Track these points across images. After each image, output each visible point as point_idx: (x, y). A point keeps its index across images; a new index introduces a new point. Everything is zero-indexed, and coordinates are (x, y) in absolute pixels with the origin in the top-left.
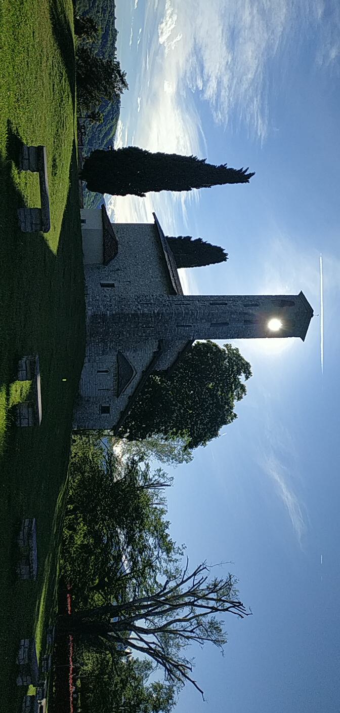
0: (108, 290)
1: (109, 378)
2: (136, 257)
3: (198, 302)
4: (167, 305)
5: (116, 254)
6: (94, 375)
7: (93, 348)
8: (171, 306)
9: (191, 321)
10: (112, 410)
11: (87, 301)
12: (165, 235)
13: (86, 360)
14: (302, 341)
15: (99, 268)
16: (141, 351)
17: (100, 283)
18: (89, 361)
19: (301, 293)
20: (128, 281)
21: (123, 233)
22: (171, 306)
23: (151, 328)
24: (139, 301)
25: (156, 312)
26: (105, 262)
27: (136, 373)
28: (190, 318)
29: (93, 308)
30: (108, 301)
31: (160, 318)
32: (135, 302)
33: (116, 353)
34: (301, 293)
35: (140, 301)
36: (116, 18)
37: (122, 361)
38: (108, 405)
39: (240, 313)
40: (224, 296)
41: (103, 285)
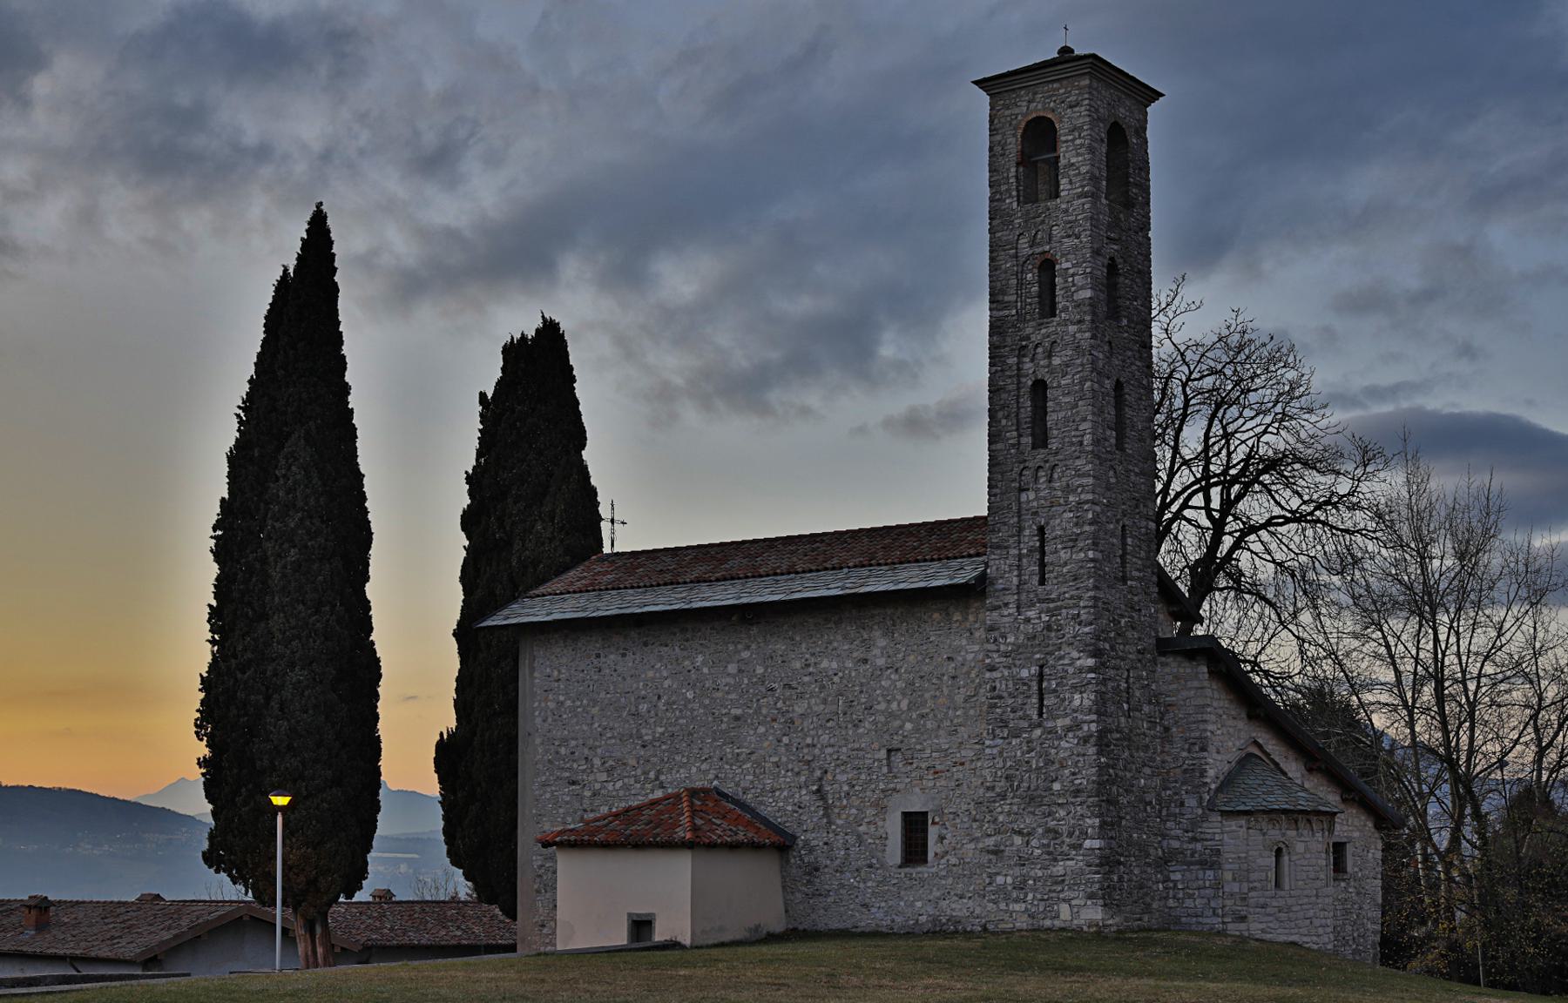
0: (942, 838)
1: (1300, 847)
2: (737, 718)
4: (1052, 613)
6: (1290, 901)
7: (1189, 903)
18: (1243, 919)
23: (1131, 680)
25: (1090, 662)
26: (782, 845)
27: (1256, 743)
34: (981, 83)
36: (1066, 50)
39: (1094, 337)
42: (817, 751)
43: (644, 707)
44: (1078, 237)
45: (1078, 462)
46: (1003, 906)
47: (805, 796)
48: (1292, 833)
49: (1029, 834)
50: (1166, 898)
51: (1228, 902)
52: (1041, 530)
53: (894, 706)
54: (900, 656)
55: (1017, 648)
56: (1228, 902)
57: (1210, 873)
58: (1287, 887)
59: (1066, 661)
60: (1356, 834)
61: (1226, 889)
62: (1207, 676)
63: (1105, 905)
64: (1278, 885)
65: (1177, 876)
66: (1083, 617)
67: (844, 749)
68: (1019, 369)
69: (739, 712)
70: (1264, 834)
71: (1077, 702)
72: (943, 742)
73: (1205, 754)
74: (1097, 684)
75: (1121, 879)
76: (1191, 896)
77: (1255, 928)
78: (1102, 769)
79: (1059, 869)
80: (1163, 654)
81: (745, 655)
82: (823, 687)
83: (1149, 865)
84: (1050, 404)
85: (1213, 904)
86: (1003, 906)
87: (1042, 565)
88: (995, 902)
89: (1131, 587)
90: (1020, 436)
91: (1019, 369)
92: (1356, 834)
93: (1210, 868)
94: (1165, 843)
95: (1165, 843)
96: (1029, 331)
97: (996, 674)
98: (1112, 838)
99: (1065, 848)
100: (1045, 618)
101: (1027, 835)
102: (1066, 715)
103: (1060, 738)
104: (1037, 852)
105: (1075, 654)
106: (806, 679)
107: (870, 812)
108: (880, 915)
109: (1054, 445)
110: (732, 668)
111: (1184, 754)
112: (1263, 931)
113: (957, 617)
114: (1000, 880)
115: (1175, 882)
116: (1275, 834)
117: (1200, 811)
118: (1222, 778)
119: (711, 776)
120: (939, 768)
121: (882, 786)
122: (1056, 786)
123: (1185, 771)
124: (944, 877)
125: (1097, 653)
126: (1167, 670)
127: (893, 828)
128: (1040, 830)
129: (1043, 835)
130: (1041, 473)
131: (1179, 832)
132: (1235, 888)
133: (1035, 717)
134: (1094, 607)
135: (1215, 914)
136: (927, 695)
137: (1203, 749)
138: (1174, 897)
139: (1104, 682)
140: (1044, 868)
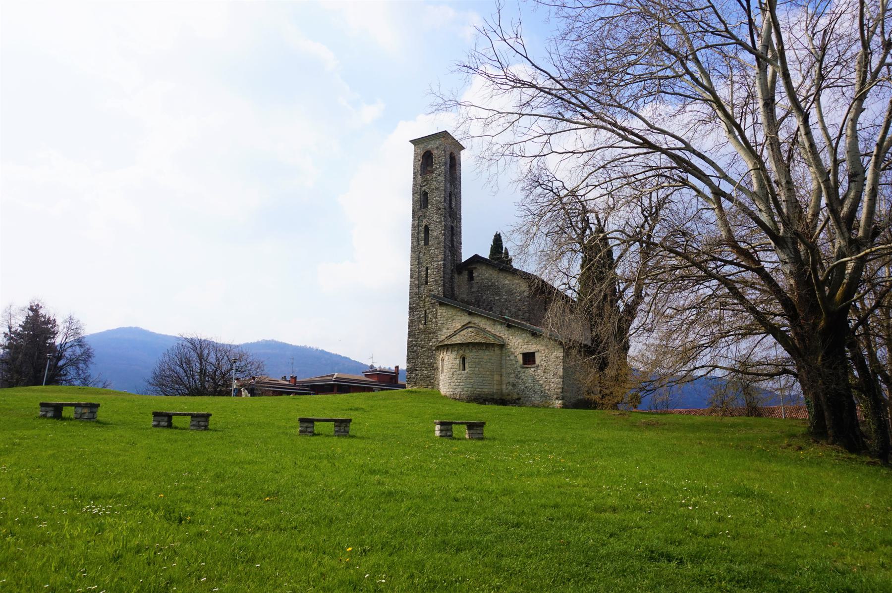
19: (414, 142)
34: (414, 142)
38: (521, 356)
75: (417, 375)
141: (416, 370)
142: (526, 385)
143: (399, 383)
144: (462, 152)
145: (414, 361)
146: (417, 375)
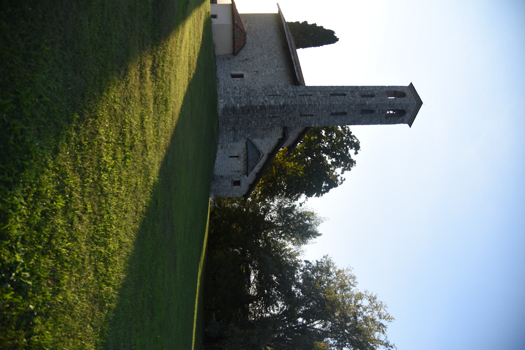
0: (238, 81)
1: (239, 162)
2: (262, 46)
3: (319, 93)
4: (292, 97)
5: (245, 44)
8: (295, 97)
9: (313, 111)
10: (243, 183)
11: (219, 93)
12: (286, 21)
13: (219, 146)
14: (409, 127)
15: (229, 59)
16: (268, 138)
17: (231, 74)
18: (222, 148)
19: (411, 84)
20: (255, 71)
21: (251, 23)
22: (295, 97)
23: (277, 118)
24: (266, 92)
25: (282, 104)
26: (235, 53)
27: (263, 155)
28: (312, 109)
29: (224, 101)
30: (238, 93)
31: (285, 109)
32: (262, 93)
33: (245, 141)
34: (411, 84)
35: (267, 92)
37: (250, 146)
38: (239, 180)
39: (358, 104)
40: (343, 87)
41: (234, 76)
42: (256, 59)
43: (263, 32)
44: (380, 101)
45: (328, 101)
46: (223, 90)
47: (245, 57)
48: (242, 160)
49: (240, 94)
50: (226, 131)
51: (225, 145)
52: (312, 95)
53: (267, 72)
54: (279, 72)
55: (284, 91)
56: (225, 145)
57: (232, 140)
58: (230, 159)
59: (281, 100)
60: (242, 189)
61: (229, 144)
62: (279, 138)
63: (224, 109)
64: (231, 157)
65: (231, 133)
66: (292, 103)
67: (257, 64)
68: (348, 91)
69: (263, 46)
70: (242, 153)
71: (272, 102)
72: (260, 80)
73: (260, 138)
74: (276, 106)
75: (230, 114)
76: (227, 136)
77: (220, 151)
78: (256, 107)
79: (232, 99)
80: (283, 128)
81: (276, 47)
82: (270, 60)
83: (234, 125)
84: (341, 96)
85: (225, 141)
86: (223, 90)
87: (303, 95)
88: (223, 88)
89: (299, 118)
90: (332, 91)
91: (348, 91)
92: (242, 189)
93: (233, 140)
94: (239, 130)
95: (239, 130)
96: (357, 93)
97: (277, 87)
98: (240, 111)
99: (237, 100)
100: (291, 96)
101: (240, 93)
102: (268, 99)
103: (263, 99)
104: (236, 95)
105: (283, 101)
106: (272, 57)
107: (243, 69)
108: (219, 70)
109: (332, 97)
110: (273, 45)
111: (260, 134)
112: (219, 153)
113: (289, 82)
114: (229, 89)
115: (230, 132)
116: (242, 155)
117: (247, 137)
118: (255, 144)
119: (249, 42)
120: (254, 80)
121: (249, 70)
122: (251, 98)
123: (256, 134)
124: (229, 81)
125: (284, 106)
126: (280, 129)
127: (240, 72)
128: (241, 96)
129: (240, 96)
130: (324, 95)
131: (242, 133)
132: (229, 146)
133: (267, 94)
134: (295, 105)
135: (223, 141)
136: (271, 77)
137: (261, 138)
138: (226, 132)
139: (277, 108)
140: (232, 97)
141: (234, 114)
142: (222, 182)
143: (306, 85)
144: (407, 125)
145: (241, 112)
146: (230, 114)
